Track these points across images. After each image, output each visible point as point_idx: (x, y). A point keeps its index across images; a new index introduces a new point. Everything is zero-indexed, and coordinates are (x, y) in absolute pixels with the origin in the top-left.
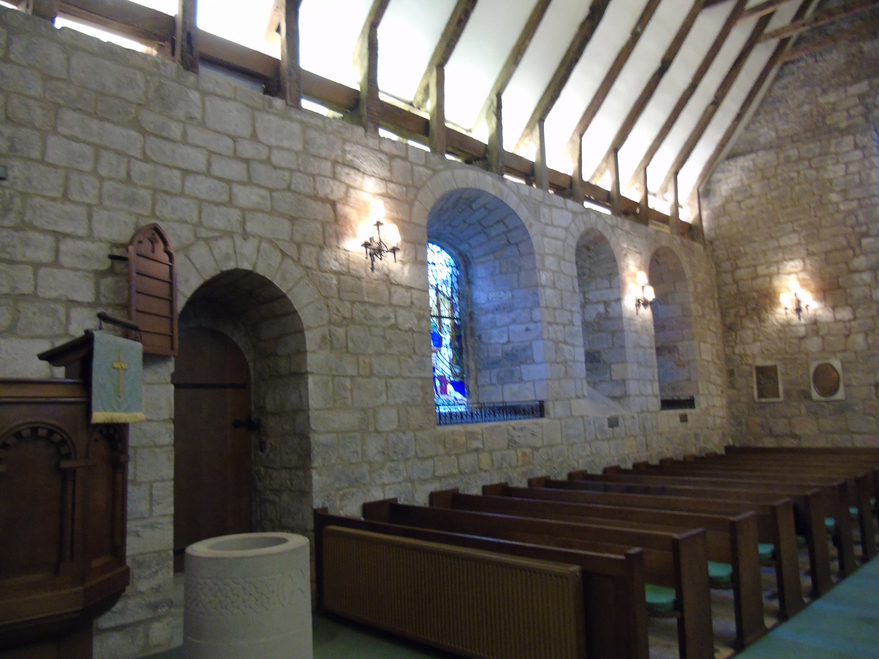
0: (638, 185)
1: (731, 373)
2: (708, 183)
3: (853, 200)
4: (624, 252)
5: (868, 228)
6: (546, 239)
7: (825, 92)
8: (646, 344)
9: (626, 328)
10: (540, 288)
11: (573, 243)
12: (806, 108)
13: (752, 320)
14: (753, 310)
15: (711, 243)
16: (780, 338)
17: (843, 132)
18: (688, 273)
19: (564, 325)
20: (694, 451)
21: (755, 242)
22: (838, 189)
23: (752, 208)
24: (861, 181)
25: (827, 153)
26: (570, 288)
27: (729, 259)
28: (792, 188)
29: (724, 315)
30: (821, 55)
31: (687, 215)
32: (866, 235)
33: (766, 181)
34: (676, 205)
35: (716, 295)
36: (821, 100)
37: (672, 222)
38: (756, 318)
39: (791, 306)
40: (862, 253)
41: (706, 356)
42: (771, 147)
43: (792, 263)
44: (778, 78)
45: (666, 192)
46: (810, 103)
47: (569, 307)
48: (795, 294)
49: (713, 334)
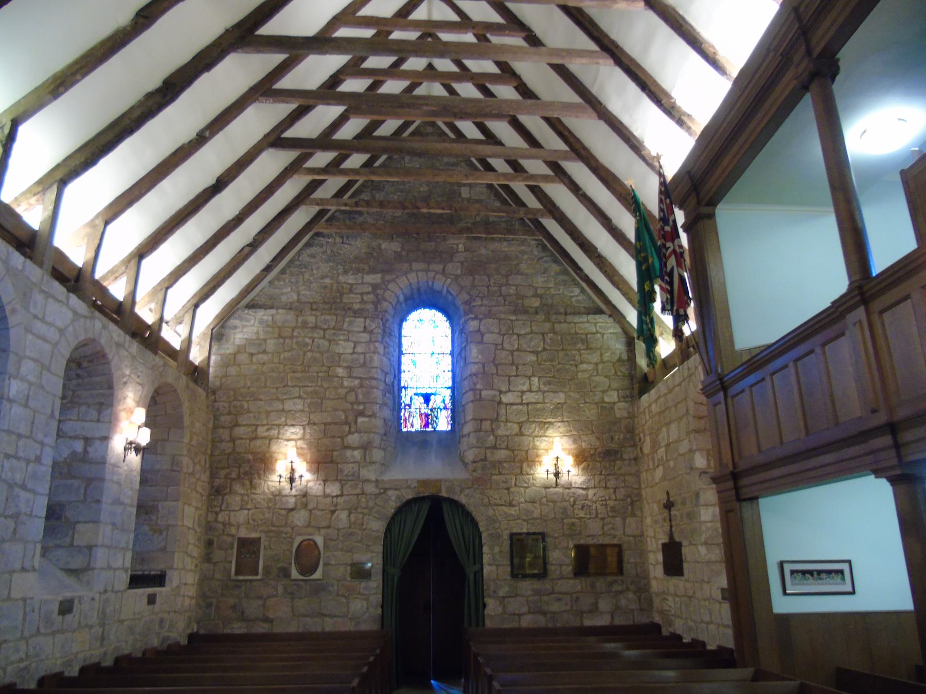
0: (153, 306)
1: (210, 543)
2: (223, 327)
3: (357, 378)
4: (125, 380)
6: (30, 337)
7: (345, 272)
8: (128, 501)
9: (108, 476)
10: (5, 402)
11: (66, 352)
12: (328, 281)
13: (243, 485)
14: (246, 473)
15: (214, 392)
16: (269, 508)
17: (357, 313)
18: (187, 420)
19: (28, 461)
20: (155, 642)
21: (261, 400)
23: (264, 364)
24: (364, 363)
26: (49, 411)
27: (229, 413)
28: (305, 354)
29: (213, 476)
30: (348, 237)
31: (197, 356)
32: (362, 414)
33: (282, 341)
34: (188, 342)
35: (209, 452)
37: (180, 358)
38: (247, 483)
39: (286, 474)
40: (356, 431)
41: (188, 522)
42: (291, 309)
43: (293, 430)
44: (308, 245)
45: (180, 323)
46: (332, 278)
47: (40, 436)
48: (290, 462)
49: (199, 496)
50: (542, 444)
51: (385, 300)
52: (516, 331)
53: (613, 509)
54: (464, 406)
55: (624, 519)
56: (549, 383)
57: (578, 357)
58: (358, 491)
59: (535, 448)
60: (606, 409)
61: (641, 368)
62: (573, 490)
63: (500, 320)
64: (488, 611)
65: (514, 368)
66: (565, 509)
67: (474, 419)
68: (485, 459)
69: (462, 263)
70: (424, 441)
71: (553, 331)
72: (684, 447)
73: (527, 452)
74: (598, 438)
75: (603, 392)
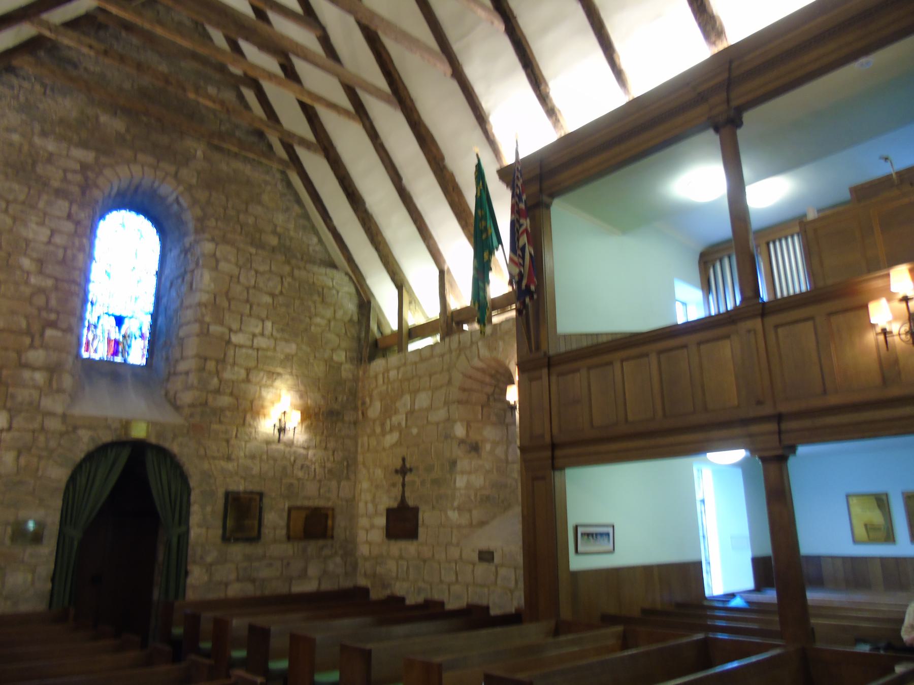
3: (49, 276)
5: (58, 318)
7: (44, 134)
17: (60, 193)
22: (35, 255)
25: (33, 207)
30: (52, 90)
32: (53, 325)
36: (37, 141)
50: (268, 395)
51: (97, 187)
52: (254, 265)
53: (330, 471)
54: (182, 339)
55: (339, 483)
56: (283, 330)
57: (313, 309)
58: (36, 425)
59: (261, 397)
60: (333, 367)
61: (373, 334)
62: (294, 449)
63: (238, 250)
64: (191, 580)
65: (248, 307)
66: (284, 468)
67: (198, 356)
68: (206, 404)
69: (199, 173)
70: (112, 372)
71: (292, 275)
72: (440, 414)
73: (252, 402)
74: (323, 397)
75: (333, 350)
